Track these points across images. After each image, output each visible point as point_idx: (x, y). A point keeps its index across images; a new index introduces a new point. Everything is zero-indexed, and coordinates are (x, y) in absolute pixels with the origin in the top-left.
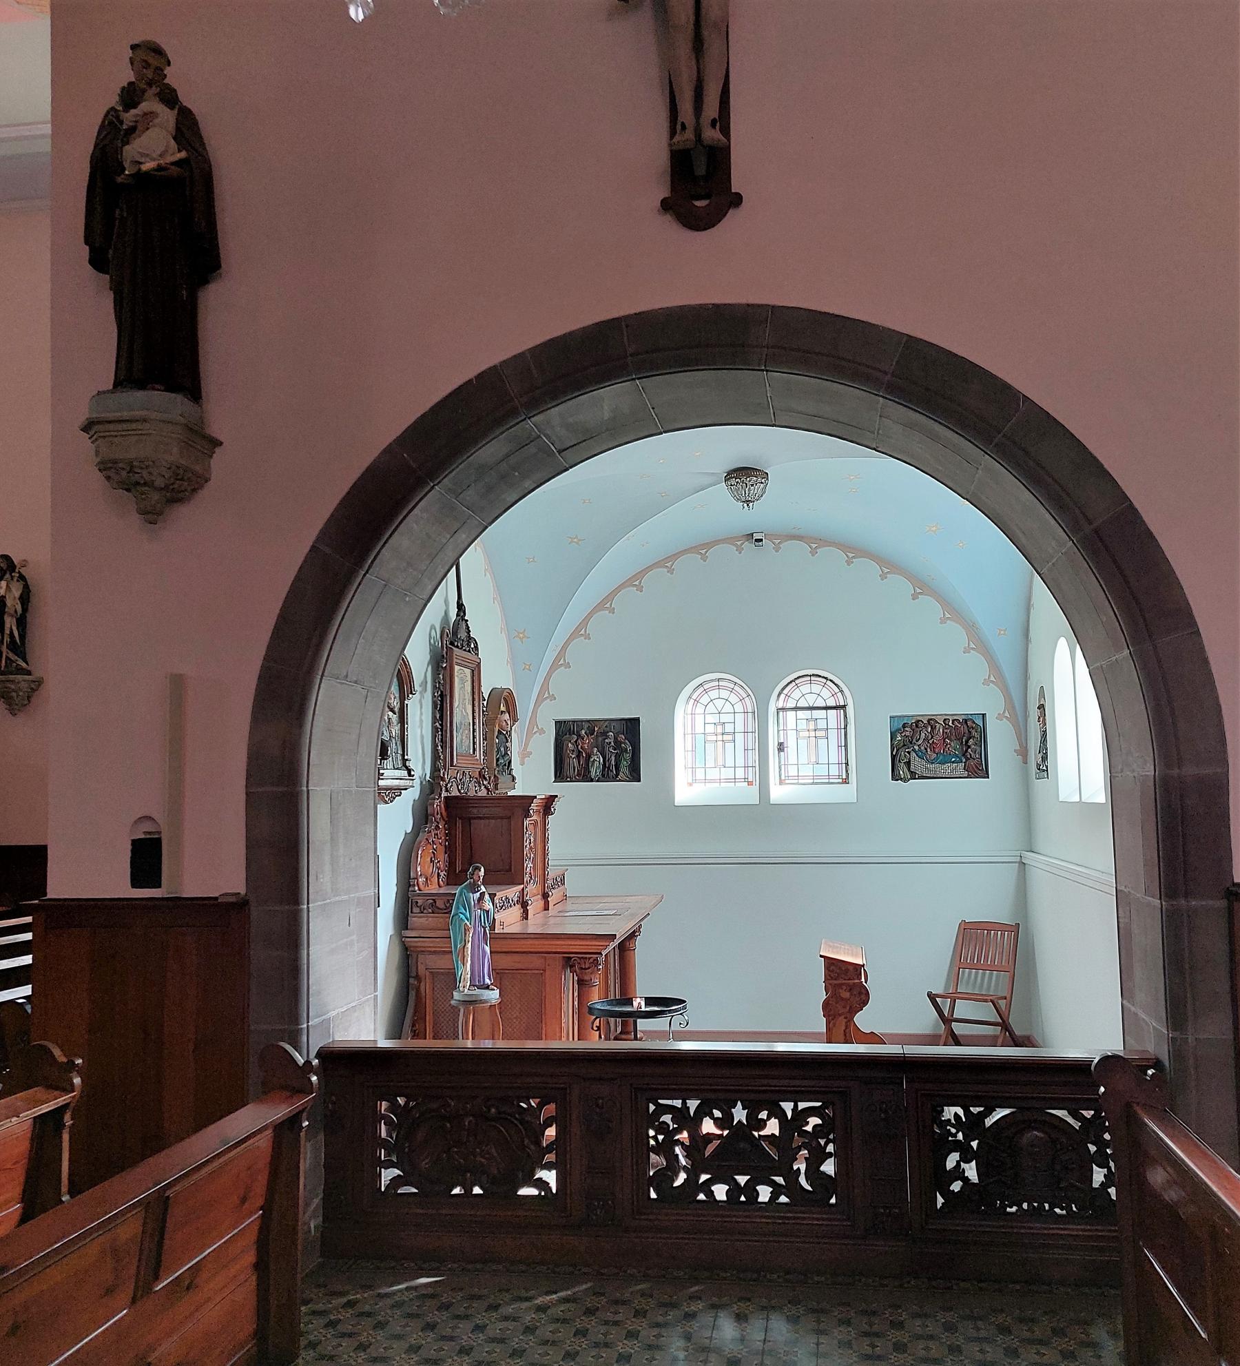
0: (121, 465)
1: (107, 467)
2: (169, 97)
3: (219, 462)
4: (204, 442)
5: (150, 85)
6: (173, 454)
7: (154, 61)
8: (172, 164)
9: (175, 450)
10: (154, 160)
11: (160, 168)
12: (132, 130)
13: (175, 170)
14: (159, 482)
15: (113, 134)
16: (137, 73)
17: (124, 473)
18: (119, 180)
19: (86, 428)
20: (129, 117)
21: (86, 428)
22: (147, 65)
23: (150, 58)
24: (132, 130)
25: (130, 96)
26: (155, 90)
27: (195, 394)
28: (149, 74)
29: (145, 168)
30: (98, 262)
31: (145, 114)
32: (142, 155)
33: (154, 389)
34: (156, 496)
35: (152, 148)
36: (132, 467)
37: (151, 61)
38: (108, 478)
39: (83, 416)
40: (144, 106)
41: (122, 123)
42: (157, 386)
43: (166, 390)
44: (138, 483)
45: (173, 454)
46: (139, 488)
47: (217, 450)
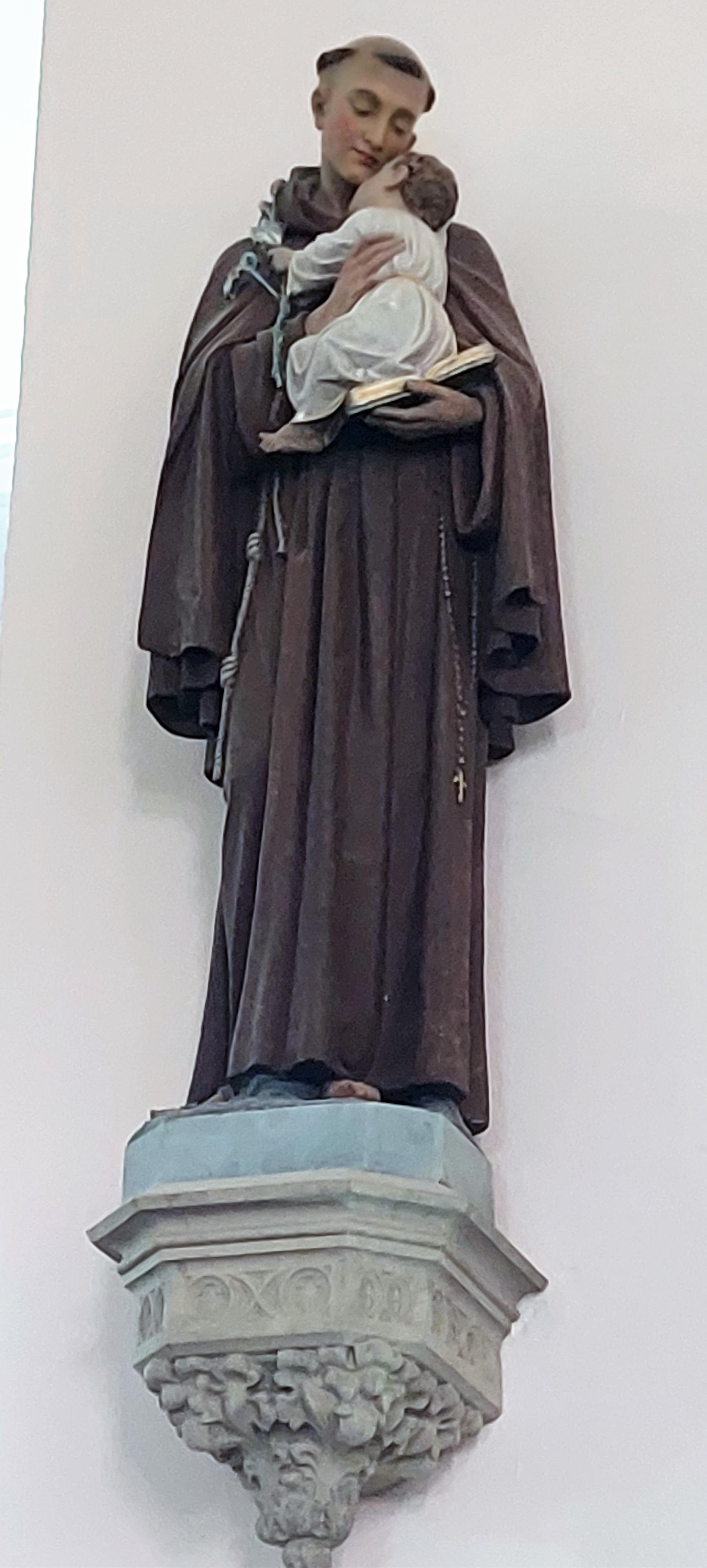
0: (235, 1361)
1: (175, 1373)
2: (431, 195)
3: (530, 1360)
4: (494, 1278)
5: (373, 163)
6: (413, 1324)
7: (391, 90)
8: (451, 382)
9: (423, 1306)
10: (395, 372)
11: (413, 398)
12: (319, 294)
13: (453, 407)
14: (361, 1422)
15: (249, 314)
16: (337, 140)
17: (236, 1393)
18: (273, 441)
19: (112, 1240)
20: (302, 265)
21: (112, 1240)
22: (371, 105)
23: (374, 91)
24: (319, 294)
25: (304, 206)
26: (389, 175)
27: (470, 1107)
28: (377, 130)
29: (361, 398)
30: (181, 698)
31: (369, 242)
32: (356, 359)
33: (350, 1093)
34: (329, 1475)
35: (383, 341)
36: (273, 1366)
37: (381, 90)
38: (178, 1410)
39: (108, 1202)
40: (365, 220)
41: (279, 277)
42: (361, 1087)
43: (385, 1098)
44: (279, 1426)
45: (413, 1324)
46: (280, 1447)
47: (527, 1307)
